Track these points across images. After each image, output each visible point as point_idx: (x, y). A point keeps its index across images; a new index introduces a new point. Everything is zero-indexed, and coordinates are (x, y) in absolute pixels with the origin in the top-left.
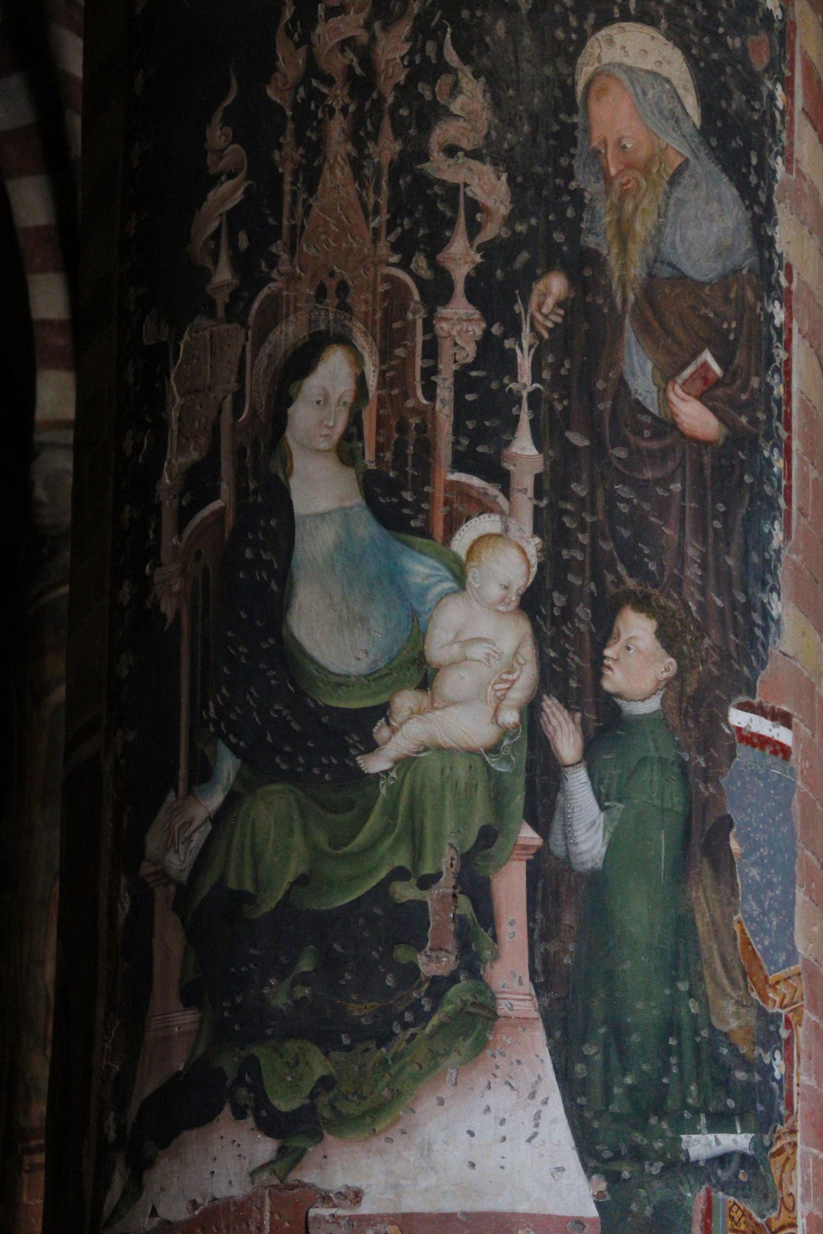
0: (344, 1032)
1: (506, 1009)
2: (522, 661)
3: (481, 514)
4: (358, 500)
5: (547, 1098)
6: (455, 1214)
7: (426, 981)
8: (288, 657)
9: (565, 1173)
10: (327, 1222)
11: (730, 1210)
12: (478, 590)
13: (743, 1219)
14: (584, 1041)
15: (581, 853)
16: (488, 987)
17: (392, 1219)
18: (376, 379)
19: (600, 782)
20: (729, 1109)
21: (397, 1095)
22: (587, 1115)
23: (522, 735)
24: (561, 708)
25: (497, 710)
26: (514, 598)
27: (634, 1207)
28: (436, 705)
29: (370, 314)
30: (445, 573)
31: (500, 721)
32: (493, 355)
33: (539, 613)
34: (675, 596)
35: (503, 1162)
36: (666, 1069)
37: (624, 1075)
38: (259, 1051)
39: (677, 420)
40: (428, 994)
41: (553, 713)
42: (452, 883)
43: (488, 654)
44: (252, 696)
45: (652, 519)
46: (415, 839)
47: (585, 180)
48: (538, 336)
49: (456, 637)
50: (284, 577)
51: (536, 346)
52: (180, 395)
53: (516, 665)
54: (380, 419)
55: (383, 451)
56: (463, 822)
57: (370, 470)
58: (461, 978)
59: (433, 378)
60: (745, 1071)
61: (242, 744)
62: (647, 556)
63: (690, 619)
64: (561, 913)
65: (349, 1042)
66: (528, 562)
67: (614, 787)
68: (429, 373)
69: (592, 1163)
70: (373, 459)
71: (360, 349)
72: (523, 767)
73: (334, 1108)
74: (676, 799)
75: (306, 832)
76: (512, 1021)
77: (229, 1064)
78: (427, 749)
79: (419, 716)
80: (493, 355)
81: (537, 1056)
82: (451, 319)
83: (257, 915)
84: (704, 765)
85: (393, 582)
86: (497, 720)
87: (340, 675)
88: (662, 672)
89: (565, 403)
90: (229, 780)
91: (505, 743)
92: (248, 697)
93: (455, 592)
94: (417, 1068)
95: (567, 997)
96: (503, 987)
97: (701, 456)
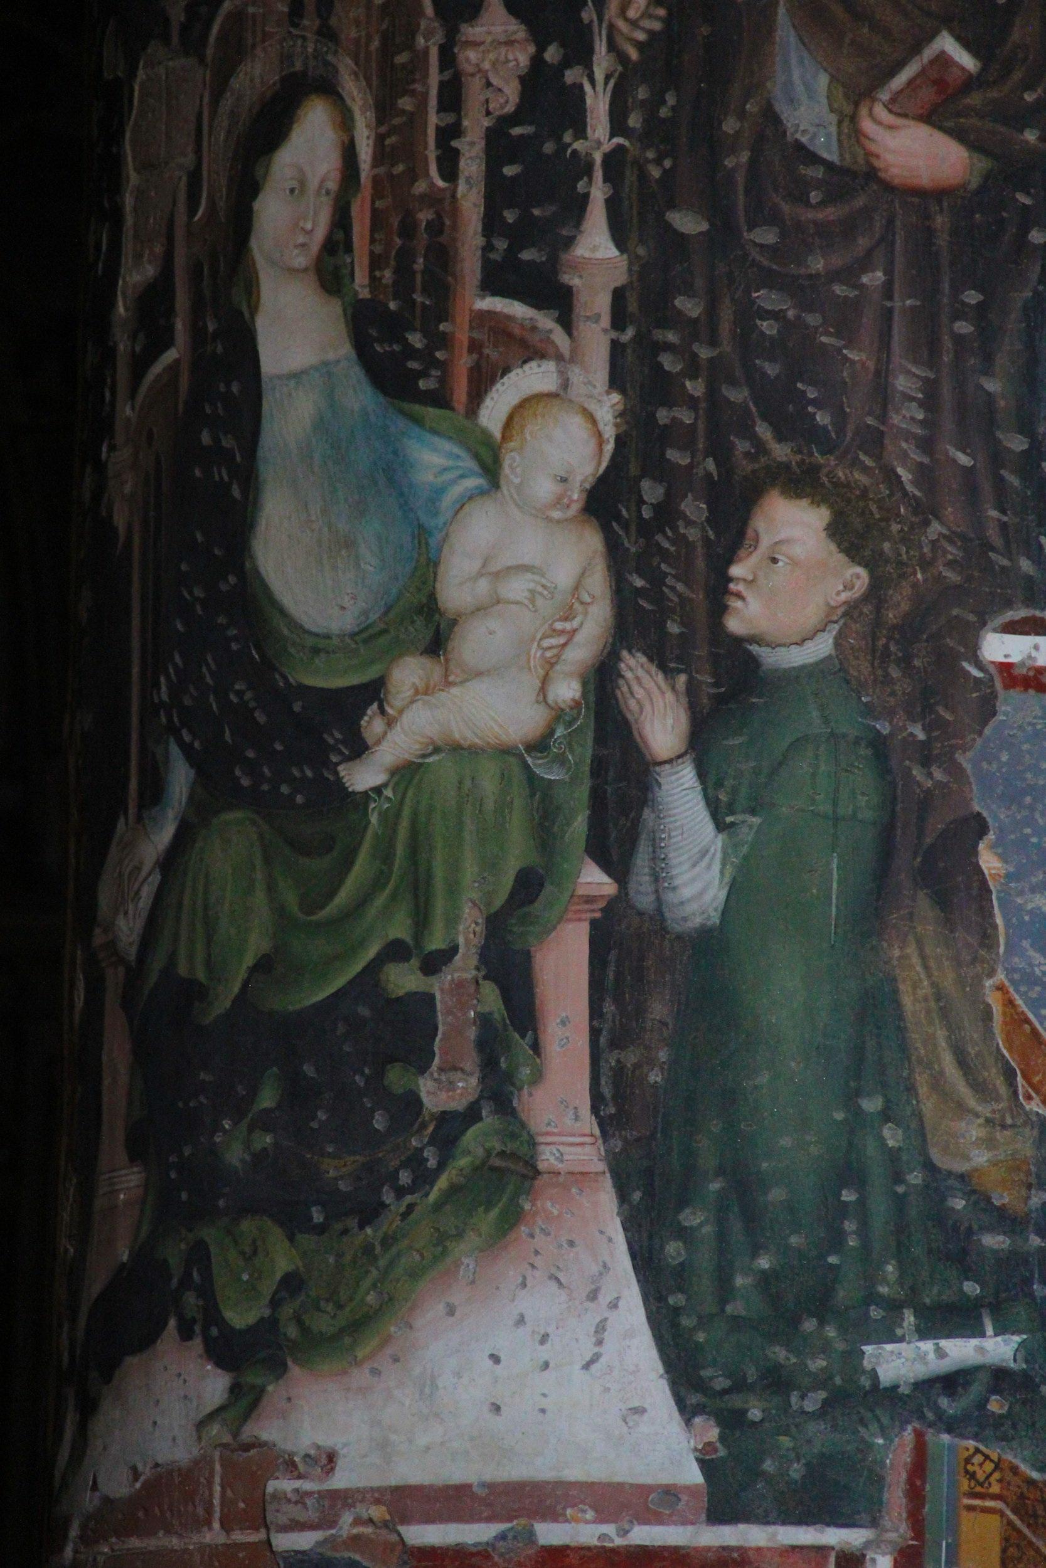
0: (316, 1203)
1: (552, 1160)
2: (587, 599)
3: (525, 362)
4: (346, 349)
5: (618, 1298)
6: (470, 1486)
7: (432, 1120)
8: (251, 604)
9: (646, 1417)
10: (289, 1501)
11: (968, 1461)
12: (519, 488)
13: (997, 1475)
14: (683, 1202)
15: (682, 903)
16: (523, 1125)
17: (376, 1495)
18: (370, 150)
19: (719, 784)
20: (968, 1298)
21: (388, 1303)
22: (686, 1322)
23: (585, 720)
24: (653, 669)
25: (545, 681)
26: (575, 497)
27: (768, 1466)
28: (451, 679)
29: (363, 40)
30: (470, 464)
31: (550, 699)
32: (549, 99)
33: (618, 517)
34: (869, 462)
35: (544, 1403)
36: (836, 1241)
37: (754, 1255)
38: (210, 1234)
39: (876, 163)
40: (432, 1141)
41: (638, 678)
42: (474, 961)
43: (532, 592)
44: (208, 665)
45: (824, 339)
46: (419, 896)
48: (622, 58)
49: (484, 566)
50: (248, 476)
51: (617, 75)
52: (135, 169)
53: (577, 605)
54: (375, 213)
55: (381, 269)
56: (490, 865)
57: (362, 300)
58: (484, 1113)
59: (455, 144)
60: (1005, 1233)
61: (197, 744)
62: (813, 402)
63: (899, 495)
64: (646, 1000)
65: (321, 1220)
66: (600, 435)
67: (744, 790)
68: (449, 133)
69: (694, 1399)
70: (366, 281)
71: (349, 102)
72: (587, 769)
73: (299, 1322)
74: (862, 800)
75: (271, 888)
76: (561, 1179)
77: (174, 1253)
78: (437, 750)
79: (426, 698)
80: (549, 99)
81: (601, 1232)
82: (483, 43)
83: (208, 1020)
84: (921, 736)
85: (391, 481)
86: (545, 697)
87: (317, 635)
88: (838, 593)
89: (667, 163)
90: (180, 803)
91: (558, 734)
92: (204, 669)
93: (482, 493)
94: (417, 1257)
95: (653, 1136)
96: (549, 1124)
97: (928, 217)
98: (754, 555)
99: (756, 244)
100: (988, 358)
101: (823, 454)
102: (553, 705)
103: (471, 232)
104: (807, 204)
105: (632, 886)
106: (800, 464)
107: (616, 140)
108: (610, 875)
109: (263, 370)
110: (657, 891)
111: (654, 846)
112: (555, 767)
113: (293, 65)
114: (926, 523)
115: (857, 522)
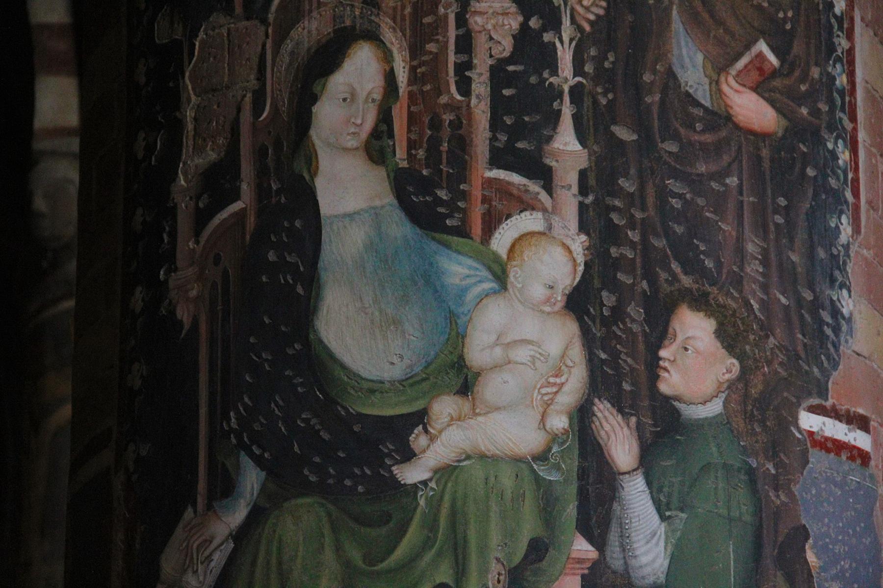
2: (571, 364)
3: (521, 212)
4: (389, 199)
12: (521, 290)
15: (641, 567)
18: (406, 75)
23: (572, 442)
26: (559, 298)
28: (477, 411)
29: (399, 8)
31: (548, 427)
32: (532, 50)
33: (588, 313)
34: (736, 294)
39: (731, 112)
41: (605, 417)
43: (533, 357)
45: (707, 214)
50: (311, 279)
51: (577, 39)
53: (563, 367)
54: (411, 115)
57: (402, 168)
62: (703, 252)
63: (752, 317)
68: (463, 68)
75: (338, 548)
80: (532, 50)
84: (773, 472)
85: (428, 282)
88: (723, 374)
89: (610, 96)
91: (554, 450)
98: (674, 344)
99: (666, 151)
100: (792, 240)
101: (710, 285)
102: (550, 431)
103: (481, 129)
104: (695, 131)
105: (608, 554)
106: (698, 290)
107: (578, 79)
108: (593, 545)
109: (322, 212)
110: (624, 558)
111: (621, 527)
112: (553, 472)
113: (344, 22)
114: (767, 337)
115: (730, 330)
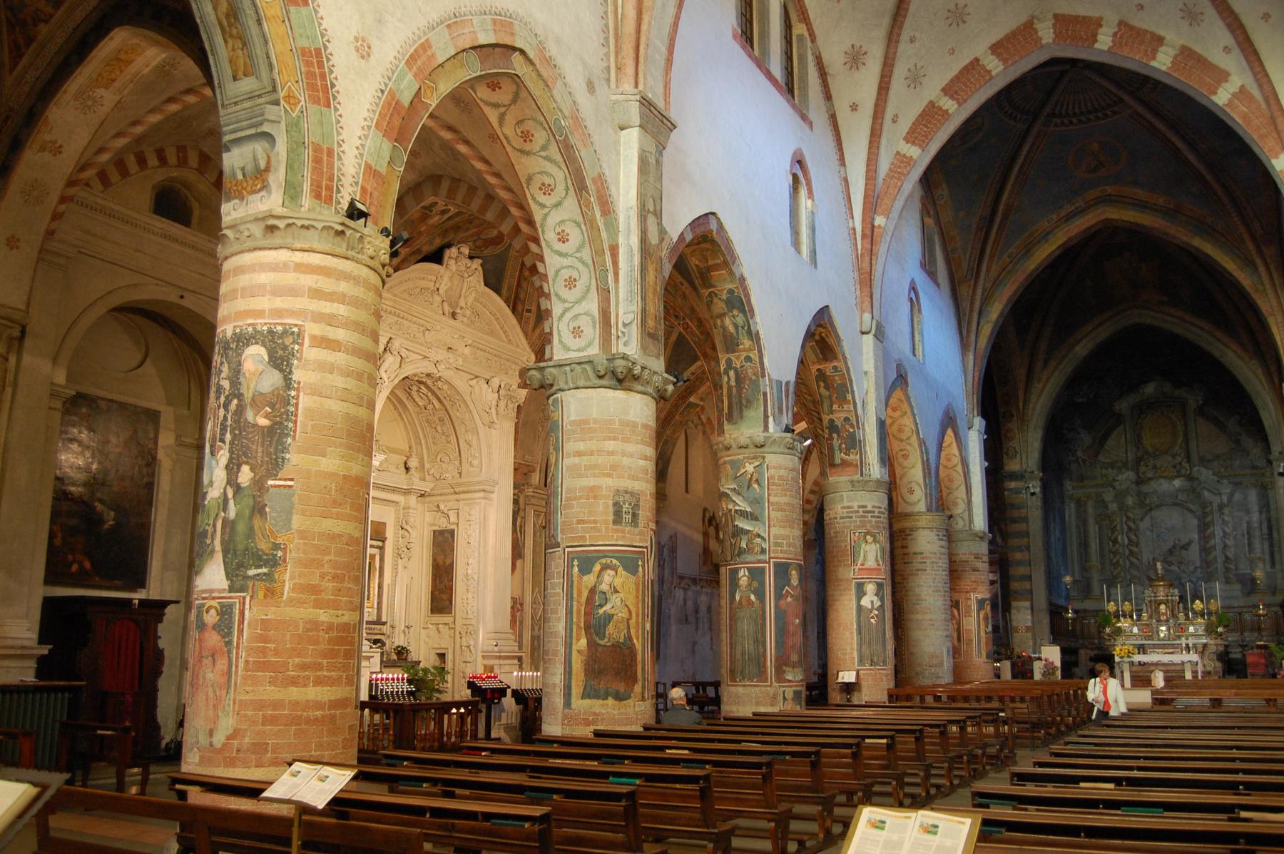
32: (225, 418)
47: (242, 379)
80: (225, 418)
